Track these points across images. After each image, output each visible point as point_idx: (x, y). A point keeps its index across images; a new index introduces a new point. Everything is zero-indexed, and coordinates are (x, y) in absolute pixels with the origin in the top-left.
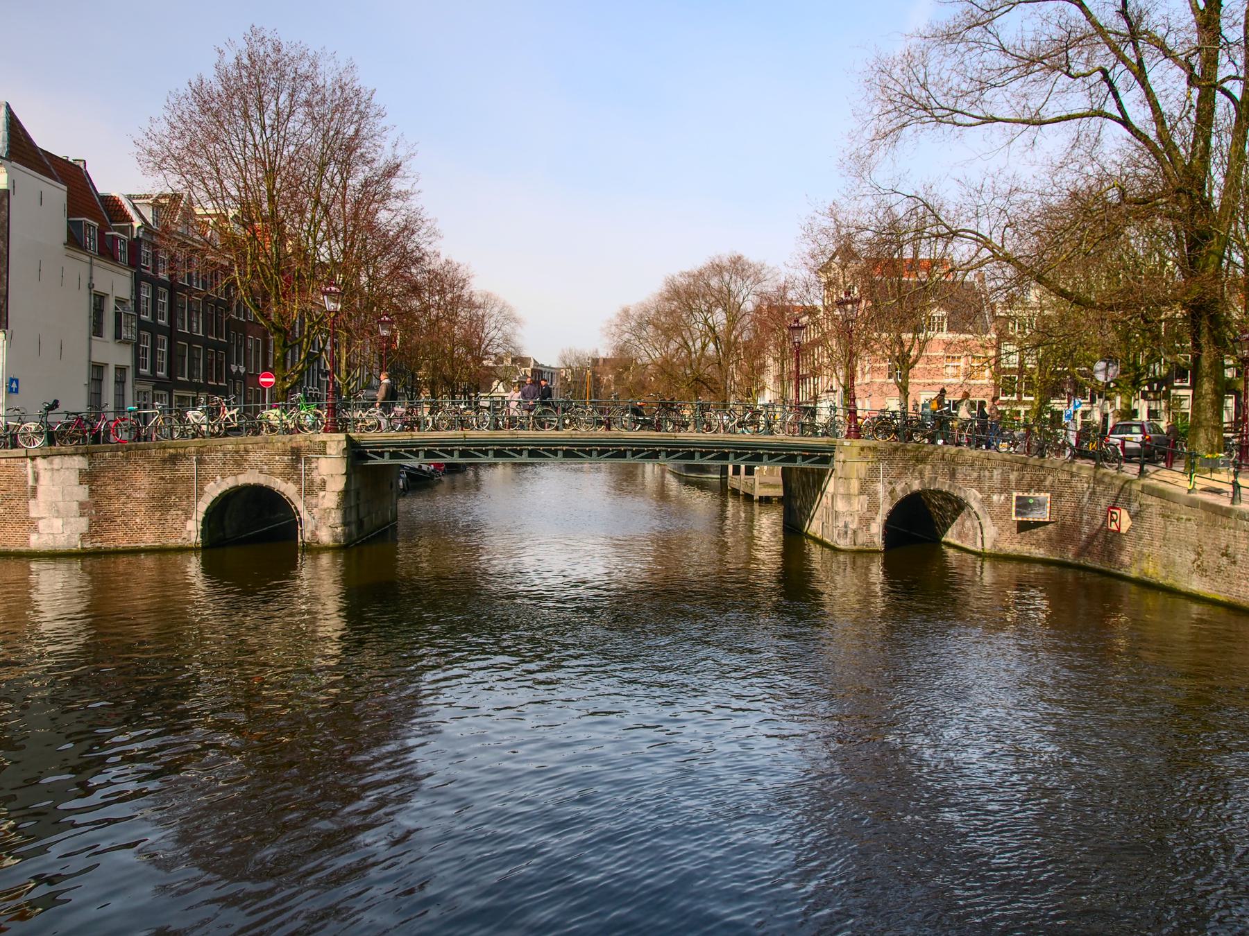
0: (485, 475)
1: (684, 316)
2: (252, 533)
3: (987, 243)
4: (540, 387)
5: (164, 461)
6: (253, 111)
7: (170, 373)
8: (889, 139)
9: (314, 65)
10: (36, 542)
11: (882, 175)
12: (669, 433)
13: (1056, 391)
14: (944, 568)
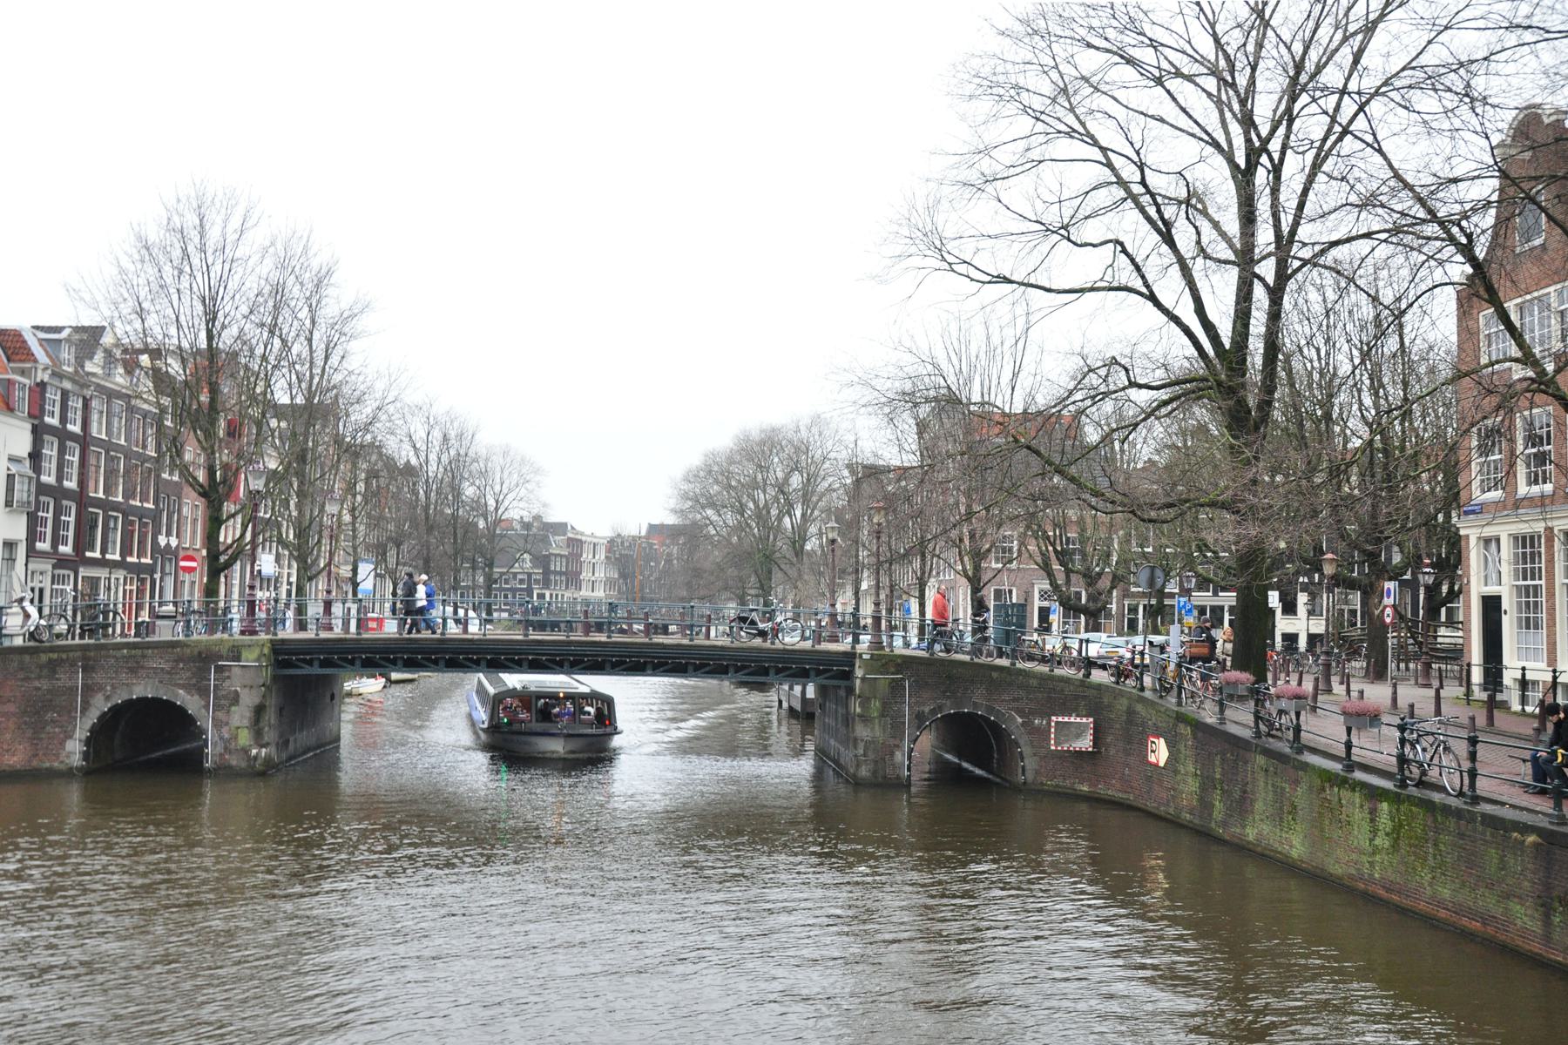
7: (76, 547)
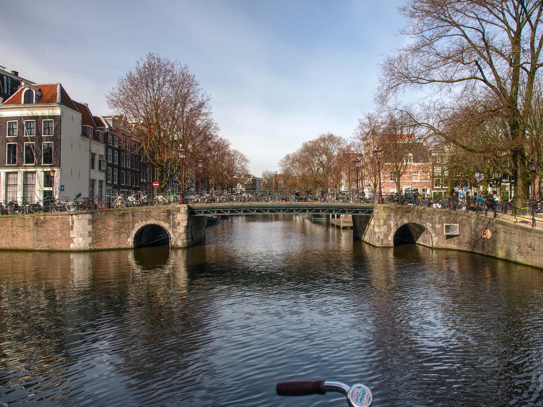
0: (235, 220)
1: (310, 158)
2: (152, 243)
3: (432, 128)
4: (253, 185)
5: (120, 216)
6: (150, 85)
7: (118, 182)
8: (393, 89)
9: (173, 66)
10: (72, 246)
11: (391, 103)
12: (310, 203)
13: (456, 184)
14: (418, 253)
